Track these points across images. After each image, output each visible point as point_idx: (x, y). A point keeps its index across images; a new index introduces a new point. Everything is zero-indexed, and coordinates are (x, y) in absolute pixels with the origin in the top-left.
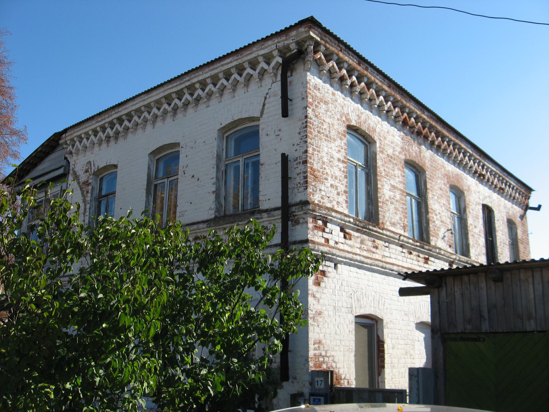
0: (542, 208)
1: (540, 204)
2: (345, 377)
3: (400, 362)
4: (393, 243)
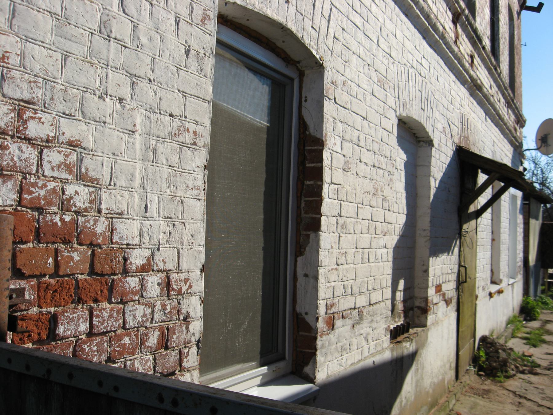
2: (150, 259)
3: (360, 216)
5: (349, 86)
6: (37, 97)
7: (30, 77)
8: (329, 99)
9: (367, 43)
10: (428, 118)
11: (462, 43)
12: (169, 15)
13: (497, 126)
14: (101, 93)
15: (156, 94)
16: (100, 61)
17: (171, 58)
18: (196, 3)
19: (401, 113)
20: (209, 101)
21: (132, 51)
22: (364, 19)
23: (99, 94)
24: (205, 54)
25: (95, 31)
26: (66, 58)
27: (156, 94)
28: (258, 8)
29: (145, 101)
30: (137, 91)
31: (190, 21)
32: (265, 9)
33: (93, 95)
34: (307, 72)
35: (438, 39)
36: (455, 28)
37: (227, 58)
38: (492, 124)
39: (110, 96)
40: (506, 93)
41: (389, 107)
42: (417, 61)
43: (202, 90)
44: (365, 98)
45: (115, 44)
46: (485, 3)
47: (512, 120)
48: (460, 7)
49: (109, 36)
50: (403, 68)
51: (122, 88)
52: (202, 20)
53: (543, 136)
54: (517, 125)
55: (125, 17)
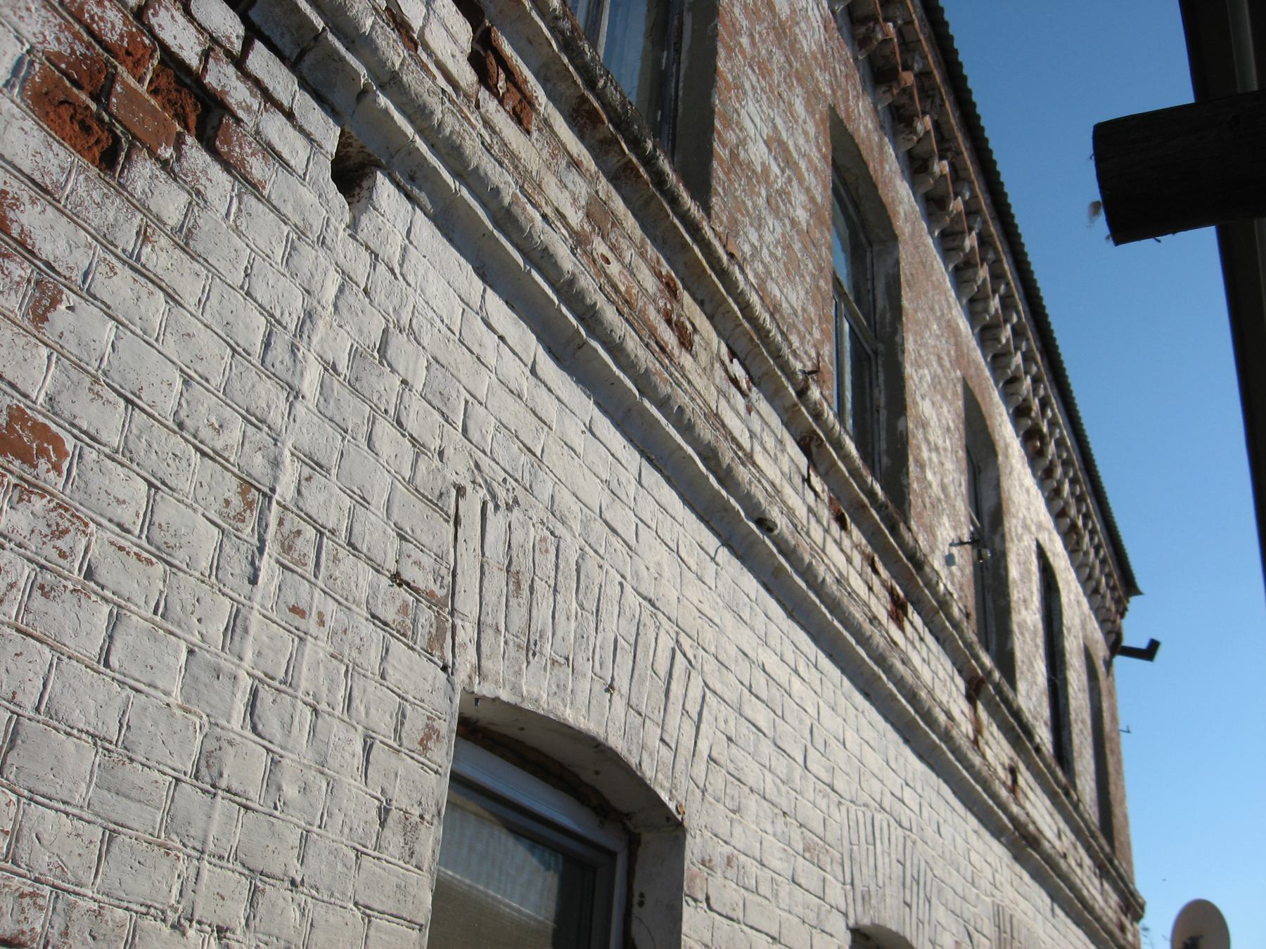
0: (1160, 654)
1: (1157, 638)
4: (774, 397)
5: (741, 868)
6: (32, 930)
7: (24, 883)
8: (695, 900)
9: (781, 765)
10: (920, 925)
11: (990, 743)
12: (352, 735)
13: (1078, 924)
14: (179, 917)
15: (303, 915)
16: (187, 843)
17: (346, 830)
18: (412, 704)
19: (859, 918)
20: (421, 926)
21: (262, 817)
22: (774, 712)
23: (172, 917)
24: (421, 817)
25: (185, 774)
26: (110, 837)
27: (303, 915)
28: (546, 706)
29: (276, 932)
30: (261, 910)
31: (395, 745)
32: (562, 708)
33: (159, 923)
34: (646, 836)
35: (937, 741)
36: (972, 712)
37: (472, 812)
38: (1069, 921)
39: (199, 923)
40: (1094, 844)
41: (832, 907)
42: (892, 794)
43: (410, 899)
44: (777, 890)
45: (226, 802)
46: (1034, 649)
47: (1113, 904)
48: (982, 666)
49: (213, 786)
50: (860, 814)
51: (228, 902)
52: (422, 740)
53: (1188, 942)
54: (1126, 915)
55: (255, 742)
